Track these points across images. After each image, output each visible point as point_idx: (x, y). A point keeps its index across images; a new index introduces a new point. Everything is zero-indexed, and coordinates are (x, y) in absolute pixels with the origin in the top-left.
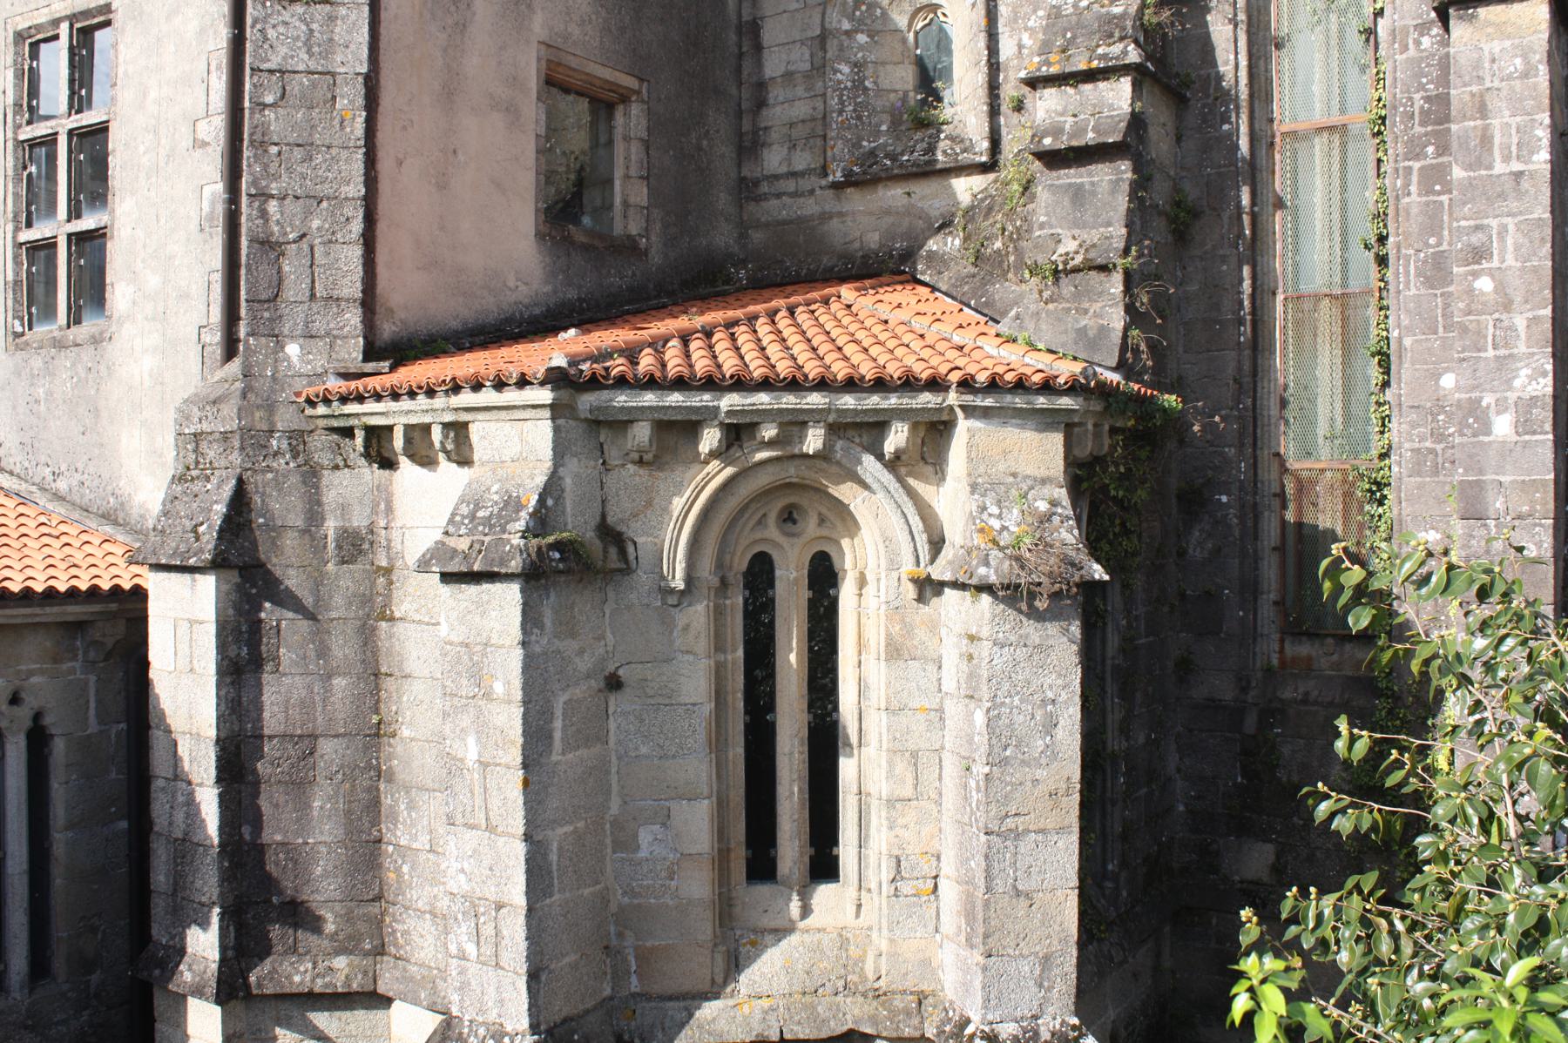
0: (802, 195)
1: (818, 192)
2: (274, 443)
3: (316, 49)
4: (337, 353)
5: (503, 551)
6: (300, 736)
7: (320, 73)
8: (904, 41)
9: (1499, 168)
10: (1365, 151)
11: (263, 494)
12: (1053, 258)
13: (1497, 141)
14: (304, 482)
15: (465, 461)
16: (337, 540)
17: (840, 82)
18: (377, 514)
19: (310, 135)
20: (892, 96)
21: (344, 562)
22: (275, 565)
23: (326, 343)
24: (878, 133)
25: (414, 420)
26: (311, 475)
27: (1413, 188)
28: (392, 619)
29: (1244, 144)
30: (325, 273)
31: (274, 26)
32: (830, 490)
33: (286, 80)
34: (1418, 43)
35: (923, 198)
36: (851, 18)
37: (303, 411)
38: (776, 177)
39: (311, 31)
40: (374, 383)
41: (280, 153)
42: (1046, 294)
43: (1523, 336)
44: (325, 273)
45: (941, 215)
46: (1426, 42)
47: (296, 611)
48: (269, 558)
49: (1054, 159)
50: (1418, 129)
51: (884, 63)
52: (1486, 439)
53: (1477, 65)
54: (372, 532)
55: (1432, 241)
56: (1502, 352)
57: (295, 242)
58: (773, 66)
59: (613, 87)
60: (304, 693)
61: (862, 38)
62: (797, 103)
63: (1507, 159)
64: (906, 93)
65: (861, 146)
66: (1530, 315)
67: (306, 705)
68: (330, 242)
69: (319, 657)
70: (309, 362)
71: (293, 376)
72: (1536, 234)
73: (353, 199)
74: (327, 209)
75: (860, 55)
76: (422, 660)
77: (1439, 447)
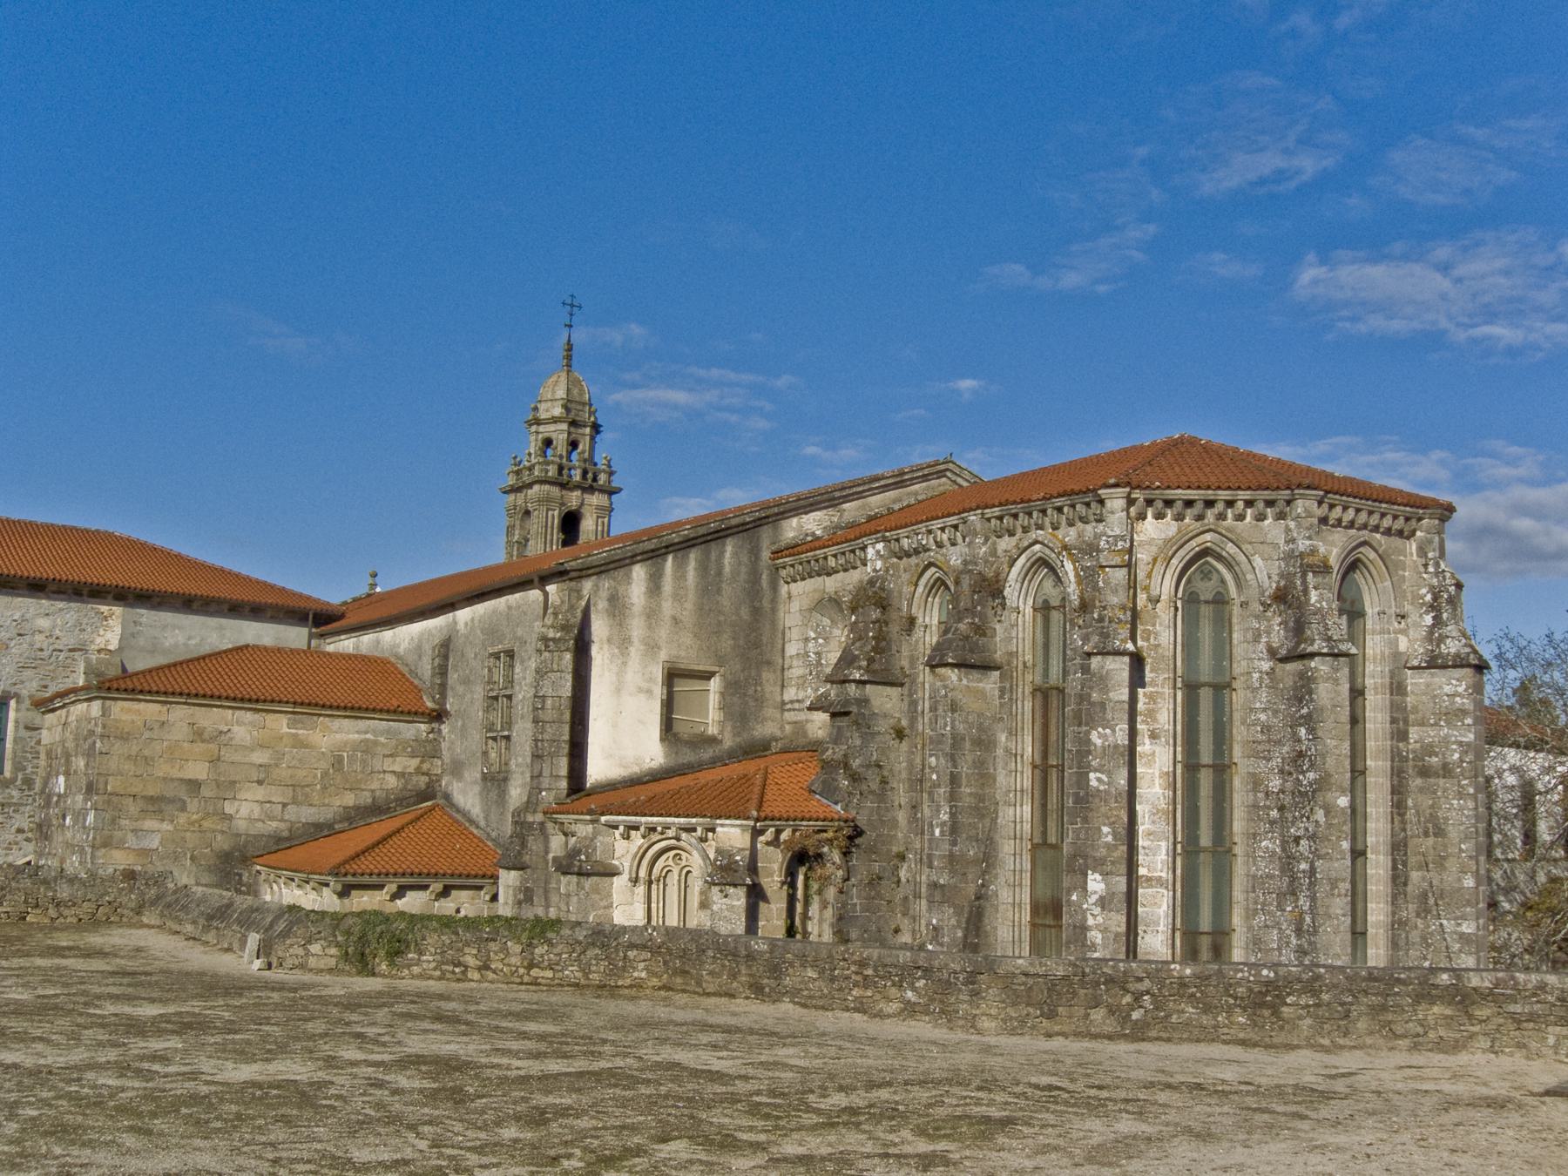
36: (815, 632)
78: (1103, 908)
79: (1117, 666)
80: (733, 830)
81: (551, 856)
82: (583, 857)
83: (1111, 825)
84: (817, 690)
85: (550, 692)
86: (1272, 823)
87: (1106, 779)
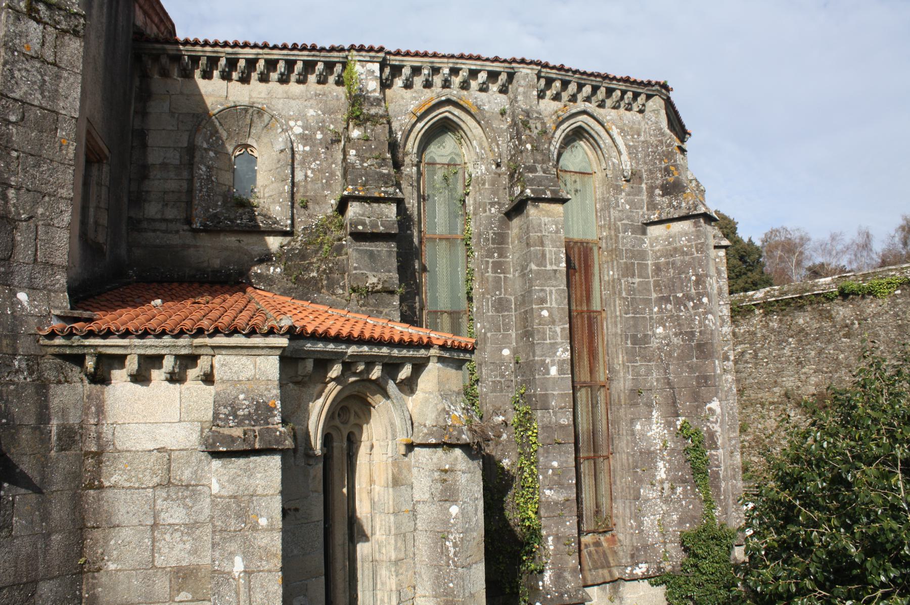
0: (171, 232)
1: (181, 232)
2: (16, 363)
3: (46, 94)
4: (53, 302)
5: (276, 436)
6: (24, 584)
7: (49, 110)
8: (230, 159)
9: (549, 267)
10: (461, 250)
11: (7, 401)
12: (367, 285)
13: (548, 256)
14: (37, 393)
16: (58, 434)
17: (201, 175)
18: (87, 415)
19: (40, 150)
21: (62, 450)
22: (12, 454)
23: (44, 295)
24: (216, 206)
26: (42, 387)
27: (490, 270)
28: (101, 487)
29: (416, 240)
30: (44, 246)
31: (19, 70)
32: (369, 399)
33: (25, 109)
34: (490, 210)
35: (248, 244)
36: (208, 143)
37: (38, 341)
38: (154, 220)
39: (44, 81)
41: (18, 157)
42: (361, 302)
43: (559, 335)
44: (44, 246)
45: (259, 255)
46: (493, 210)
47: (27, 488)
48: (9, 450)
49: (358, 237)
50: (491, 246)
51: (221, 169)
52: (548, 376)
53: (540, 225)
54: (82, 428)
55: (497, 293)
56: (552, 341)
57: (25, 220)
58: (154, 157)
60: (29, 549)
61: (212, 154)
62: (169, 181)
63: (551, 264)
65: (209, 211)
66: (562, 327)
67: (31, 559)
68: (49, 225)
69: (42, 521)
70: (36, 307)
71: (27, 316)
72: (562, 295)
73: (66, 198)
74: (48, 202)
75: (210, 162)
76: (131, 514)
77: (503, 380)
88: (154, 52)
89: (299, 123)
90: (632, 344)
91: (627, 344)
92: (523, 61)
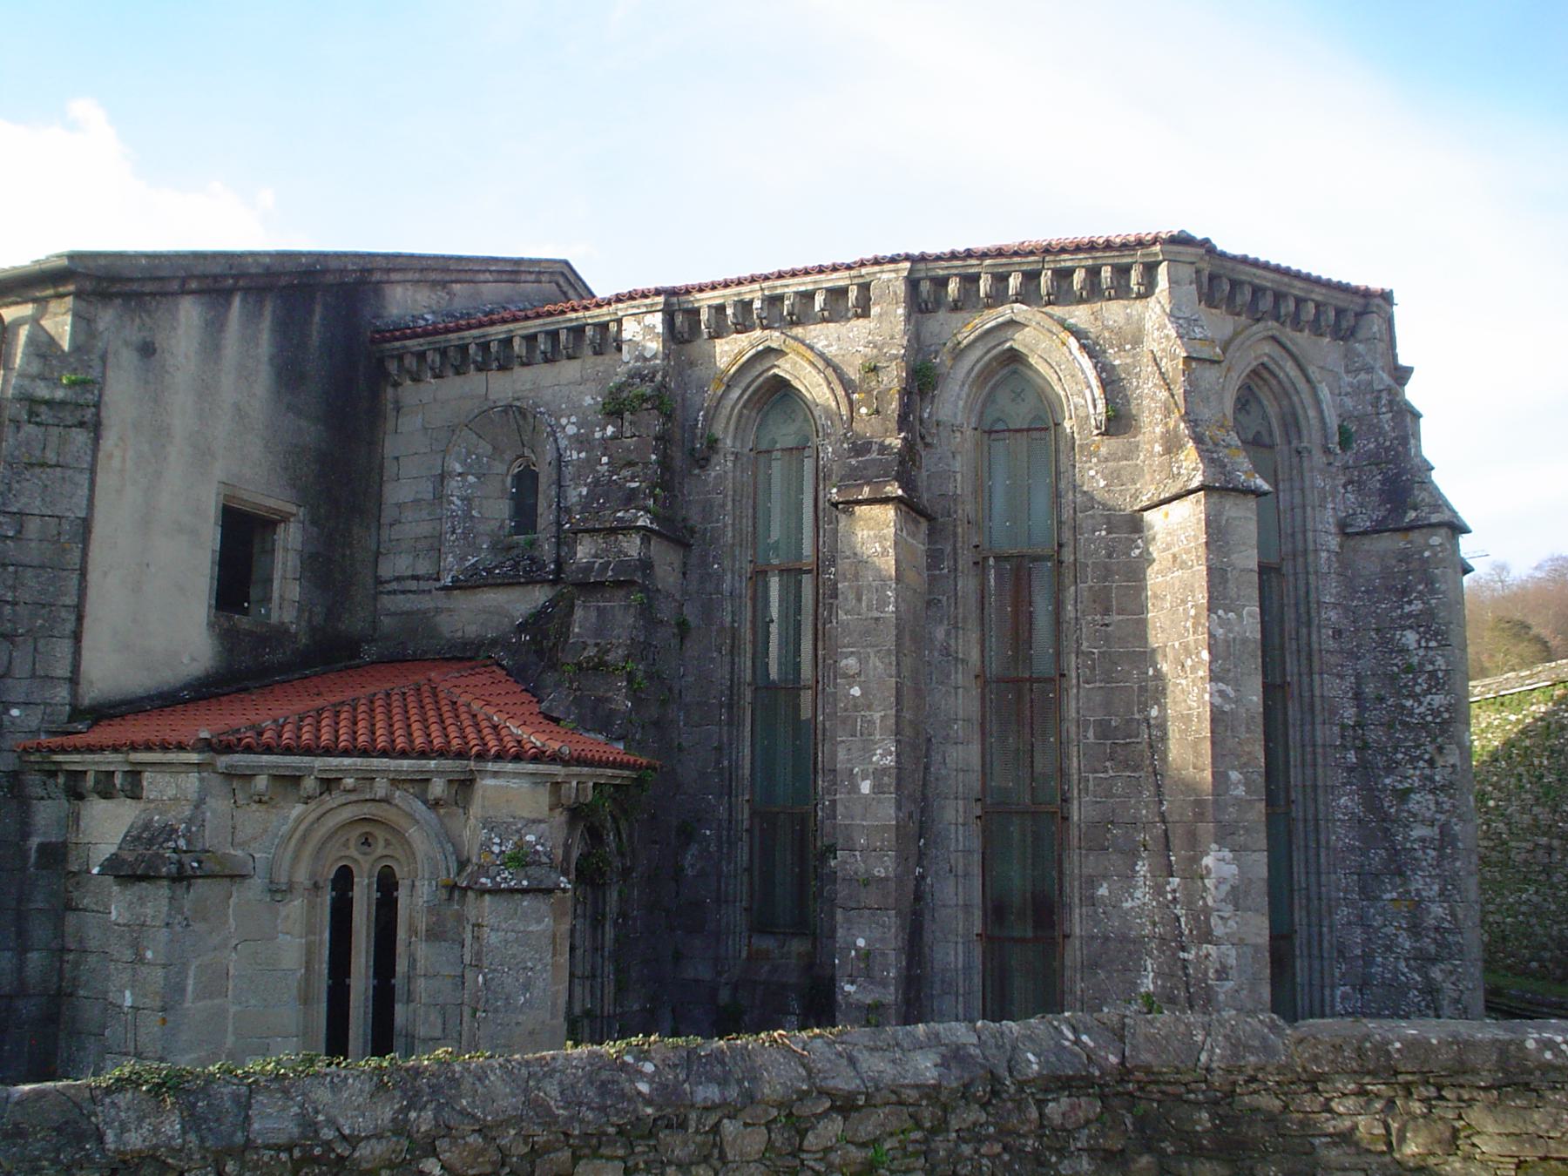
1: (434, 592)
15: (136, 796)
20: (493, 522)
25: (103, 768)
36: (464, 463)
40: (77, 740)
59: (276, 512)
64: (503, 521)
78: (1237, 908)
79: (1241, 513)
80: (514, 783)
81: (35, 842)
82: (182, 843)
83: (1240, 768)
84: (463, 559)
85: (36, 506)
86: (1351, 769)
87: (1232, 694)
88: (395, 353)
89: (573, 419)
90: (1096, 737)
91: (1086, 737)
92: (877, 262)
